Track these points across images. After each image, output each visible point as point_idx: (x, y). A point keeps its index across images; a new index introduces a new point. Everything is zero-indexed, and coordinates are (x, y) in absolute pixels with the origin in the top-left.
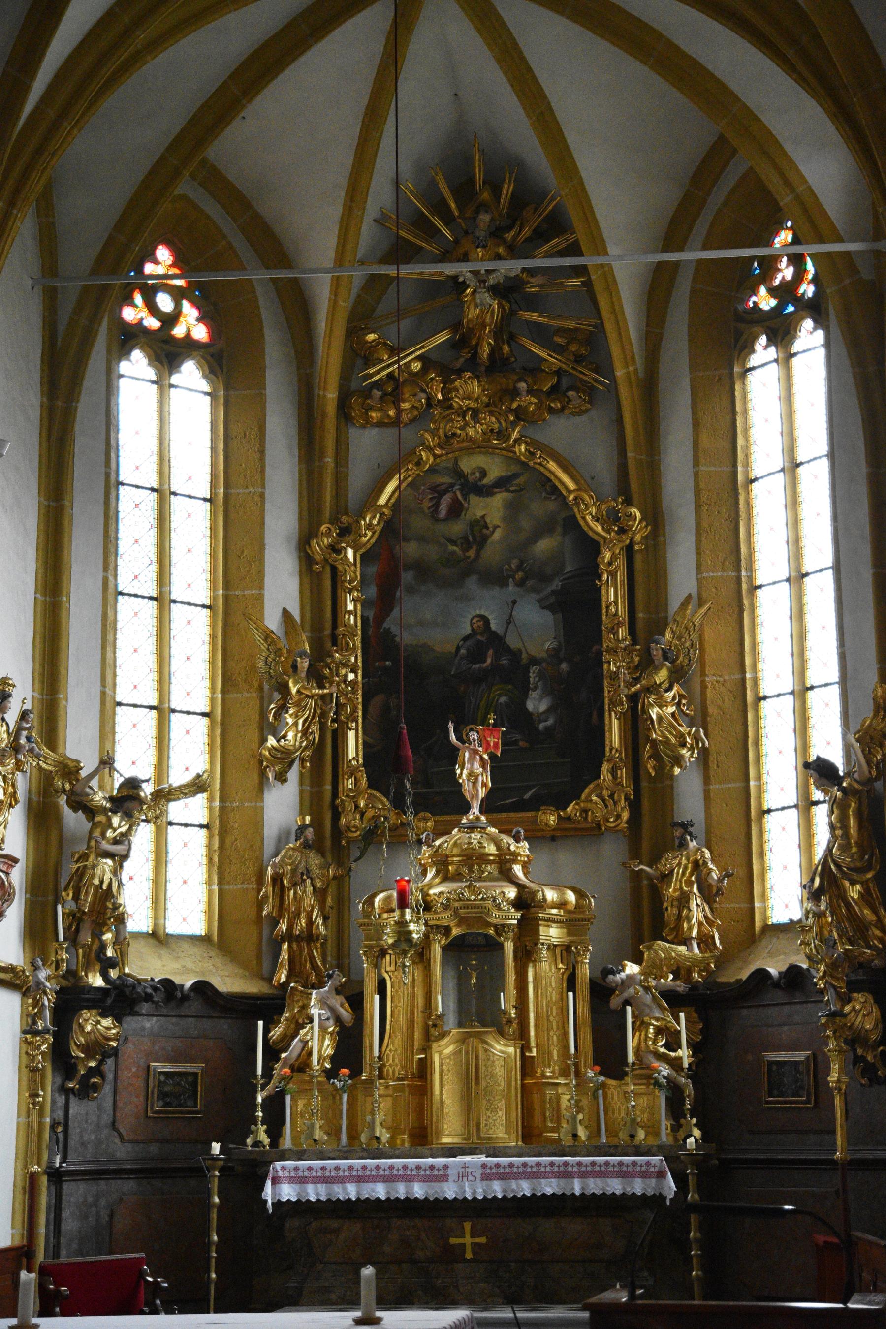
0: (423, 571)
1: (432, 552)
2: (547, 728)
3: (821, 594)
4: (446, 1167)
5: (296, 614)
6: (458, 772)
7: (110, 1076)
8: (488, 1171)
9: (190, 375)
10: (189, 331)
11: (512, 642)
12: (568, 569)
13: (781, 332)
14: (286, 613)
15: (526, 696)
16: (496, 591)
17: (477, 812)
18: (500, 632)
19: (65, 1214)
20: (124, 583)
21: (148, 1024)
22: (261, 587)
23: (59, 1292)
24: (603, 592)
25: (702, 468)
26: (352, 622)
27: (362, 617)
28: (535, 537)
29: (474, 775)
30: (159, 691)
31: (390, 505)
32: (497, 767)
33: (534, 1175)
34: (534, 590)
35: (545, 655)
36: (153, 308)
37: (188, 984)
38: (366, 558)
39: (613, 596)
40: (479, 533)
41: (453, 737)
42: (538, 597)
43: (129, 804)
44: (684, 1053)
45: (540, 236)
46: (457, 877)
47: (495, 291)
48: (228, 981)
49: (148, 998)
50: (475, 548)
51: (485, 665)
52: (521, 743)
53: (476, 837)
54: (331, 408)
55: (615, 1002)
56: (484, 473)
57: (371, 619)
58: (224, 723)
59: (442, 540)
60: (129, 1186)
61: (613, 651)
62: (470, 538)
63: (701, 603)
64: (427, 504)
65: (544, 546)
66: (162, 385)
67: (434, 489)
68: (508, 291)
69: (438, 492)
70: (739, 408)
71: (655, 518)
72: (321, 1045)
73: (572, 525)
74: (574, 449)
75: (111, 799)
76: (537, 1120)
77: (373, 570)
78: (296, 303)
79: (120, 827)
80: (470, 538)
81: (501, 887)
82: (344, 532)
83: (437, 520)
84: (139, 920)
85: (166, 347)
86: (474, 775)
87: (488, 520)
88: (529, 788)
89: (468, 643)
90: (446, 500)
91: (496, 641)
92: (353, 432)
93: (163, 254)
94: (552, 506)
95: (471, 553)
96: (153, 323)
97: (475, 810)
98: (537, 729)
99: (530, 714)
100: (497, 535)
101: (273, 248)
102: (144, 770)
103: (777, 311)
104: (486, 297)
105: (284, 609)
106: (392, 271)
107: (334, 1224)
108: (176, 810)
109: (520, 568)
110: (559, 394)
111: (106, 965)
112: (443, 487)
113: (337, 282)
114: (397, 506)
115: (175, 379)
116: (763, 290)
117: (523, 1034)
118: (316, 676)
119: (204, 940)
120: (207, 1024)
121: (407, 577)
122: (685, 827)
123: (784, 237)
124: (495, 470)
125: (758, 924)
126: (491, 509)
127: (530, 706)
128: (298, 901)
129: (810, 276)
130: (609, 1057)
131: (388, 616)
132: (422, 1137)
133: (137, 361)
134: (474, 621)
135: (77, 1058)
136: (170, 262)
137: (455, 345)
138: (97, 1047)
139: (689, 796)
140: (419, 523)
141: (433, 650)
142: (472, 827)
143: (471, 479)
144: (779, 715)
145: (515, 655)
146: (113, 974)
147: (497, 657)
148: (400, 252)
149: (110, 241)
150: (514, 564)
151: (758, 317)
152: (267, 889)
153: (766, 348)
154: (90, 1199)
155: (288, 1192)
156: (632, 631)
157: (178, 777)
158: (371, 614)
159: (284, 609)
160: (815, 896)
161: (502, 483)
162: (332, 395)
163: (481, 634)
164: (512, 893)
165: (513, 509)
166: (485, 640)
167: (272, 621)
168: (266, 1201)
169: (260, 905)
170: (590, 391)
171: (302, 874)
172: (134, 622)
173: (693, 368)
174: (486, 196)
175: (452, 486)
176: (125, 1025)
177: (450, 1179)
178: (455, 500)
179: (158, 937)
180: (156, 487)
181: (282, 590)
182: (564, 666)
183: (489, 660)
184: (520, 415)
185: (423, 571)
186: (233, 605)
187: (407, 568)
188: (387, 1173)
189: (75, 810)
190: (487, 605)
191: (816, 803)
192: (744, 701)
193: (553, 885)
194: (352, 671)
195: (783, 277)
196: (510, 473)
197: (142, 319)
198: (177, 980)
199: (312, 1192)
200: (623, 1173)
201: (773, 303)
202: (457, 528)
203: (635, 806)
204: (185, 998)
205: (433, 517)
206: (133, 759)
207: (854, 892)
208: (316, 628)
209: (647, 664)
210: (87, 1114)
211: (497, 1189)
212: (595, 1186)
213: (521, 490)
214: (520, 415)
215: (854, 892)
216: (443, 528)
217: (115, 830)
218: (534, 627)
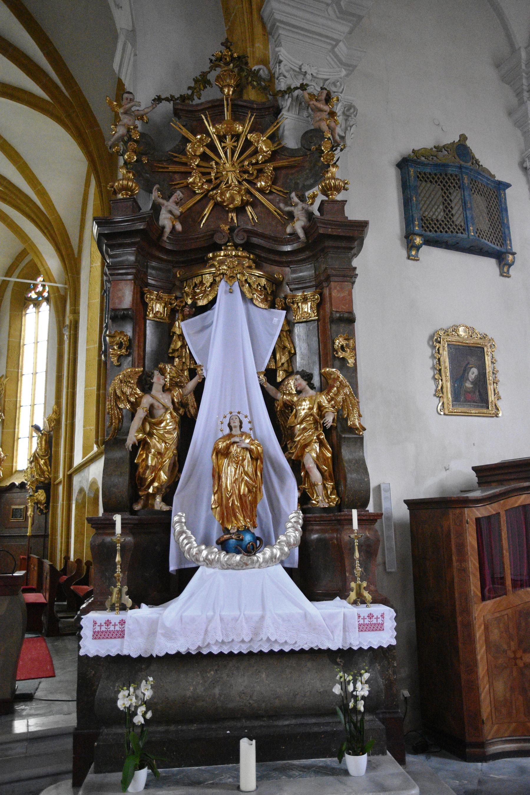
9: (45, 307)
13: (37, 304)
63: (6, 377)
103: (37, 299)
151: (30, 300)
160: (31, 463)
173: (10, 311)
207: (42, 462)
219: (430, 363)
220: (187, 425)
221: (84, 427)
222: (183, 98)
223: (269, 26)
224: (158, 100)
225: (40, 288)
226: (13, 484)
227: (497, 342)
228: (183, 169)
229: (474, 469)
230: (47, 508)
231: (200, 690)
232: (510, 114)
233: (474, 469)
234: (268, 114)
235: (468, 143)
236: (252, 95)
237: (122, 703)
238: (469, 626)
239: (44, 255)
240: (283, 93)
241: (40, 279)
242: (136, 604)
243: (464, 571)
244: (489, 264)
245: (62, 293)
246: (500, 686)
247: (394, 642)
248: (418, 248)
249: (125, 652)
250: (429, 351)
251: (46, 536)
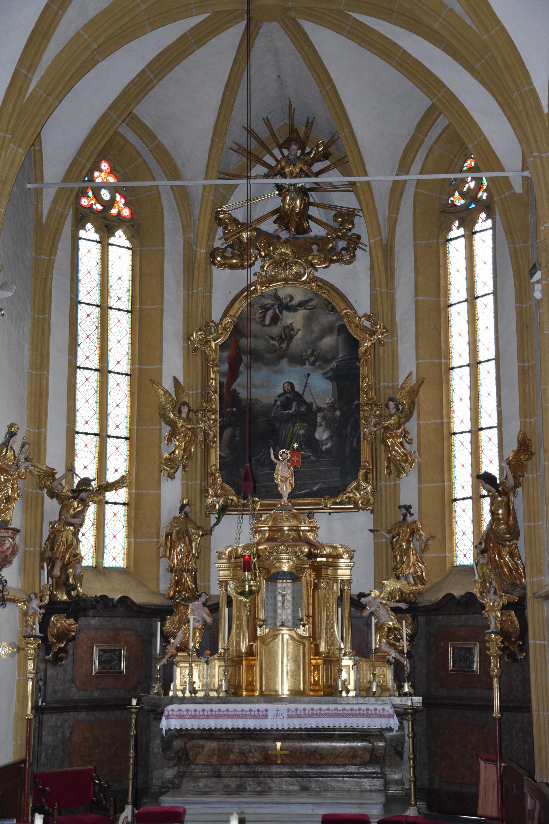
2: (326, 449)
3: (488, 374)
4: (266, 710)
5: (181, 379)
6: (276, 477)
7: (71, 652)
8: (291, 713)
9: (120, 238)
10: (119, 211)
11: (308, 398)
12: (340, 356)
14: (175, 380)
15: (315, 430)
16: (298, 368)
17: (286, 501)
18: (301, 392)
19: (45, 733)
20: (81, 361)
21: (94, 622)
22: (161, 364)
23: (45, 790)
24: (361, 368)
25: (420, 298)
26: (214, 384)
27: (220, 382)
28: (322, 336)
29: (284, 476)
30: (100, 427)
31: (237, 315)
34: (320, 367)
35: (326, 406)
36: (98, 198)
37: (117, 597)
40: (288, 334)
41: (272, 456)
42: (322, 372)
43: (83, 495)
44: (405, 644)
49: (93, 607)
50: (286, 342)
51: (291, 411)
52: (312, 458)
56: (292, 298)
57: (225, 383)
58: (137, 442)
59: (267, 337)
60: (83, 715)
62: (284, 336)
64: (258, 316)
65: (328, 341)
66: (104, 245)
67: (263, 307)
70: (441, 263)
75: (73, 491)
77: (226, 354)
79: (78, 507)
80: (284, 336)
81: (300, 545)
83: (265, 326)
84: (88, 560)
85: (106, 221)
86: (284, 476)
87: (293, 325)
88: (316, 484)
89: (281, 398)
90: (270, 314)
91: (298, 397)
95: (284, 345)
98: (321, 450)
99: (317, 441)
100: (299, 335)
102: (91, 473)
103: (465, 207)
105: (174, 377)
107: (201, 742)
108: (110, 496)
109: (312, 355)
111: (69, 588)
112: (268, 306)
115: (112, 240)
116: (457, 194)
123: (470, 163)
125: (448, 566)
126: (295, 319)
127: (317, 436)
129: (485, 187)
131: (235, 381)
133: (89, 230)
134: (286, 385)
135: (52, 642)
136: (109, 171)
138: (62, 635)
140: (255, 327)
141: (261, 402)
143: (284, 301)
144: (462, 444)
145: (309, 406)
146: (73, 593)
147: (298, 406)
150: (309, 352)
153: (458, 228)
154: (59, 724)
155: (175, 724)
157: (112, 477)
158: (225, 380)
159: (174, 377)
161: (302, 304)
163: (290, 393)
165: (309, 320)
166: (292, 396)
167: (168, 384)
168: (162, 729)
171: (183, 533)
172: (87, 385)
175: (273, 305)
176: (80, 623)
177: (269, 717)
178: (275, 314)
179: (99, 569)
180: (99, 304)
181: (173, 364)
182: (338, 413)
183: (294, 409)
185: (256, 356)
186: (143, 376)
187: (245, 353)
188: (233, 713)
189: (52, 497)
190: (292, 376)
191: (484, 496)
194: (213, 414)
195: (469, 187)
196: (307, 299)
197: (92, 204)
198: (110, 596)
201: (463, 202)
202: (276, 330)
204: (114, 606)
205: (262, 323)
206: (85, 466)
210: (57, 674)
213: (314, 308)
216: (267, 329)
217: (75, 509)
218: (320, 389)
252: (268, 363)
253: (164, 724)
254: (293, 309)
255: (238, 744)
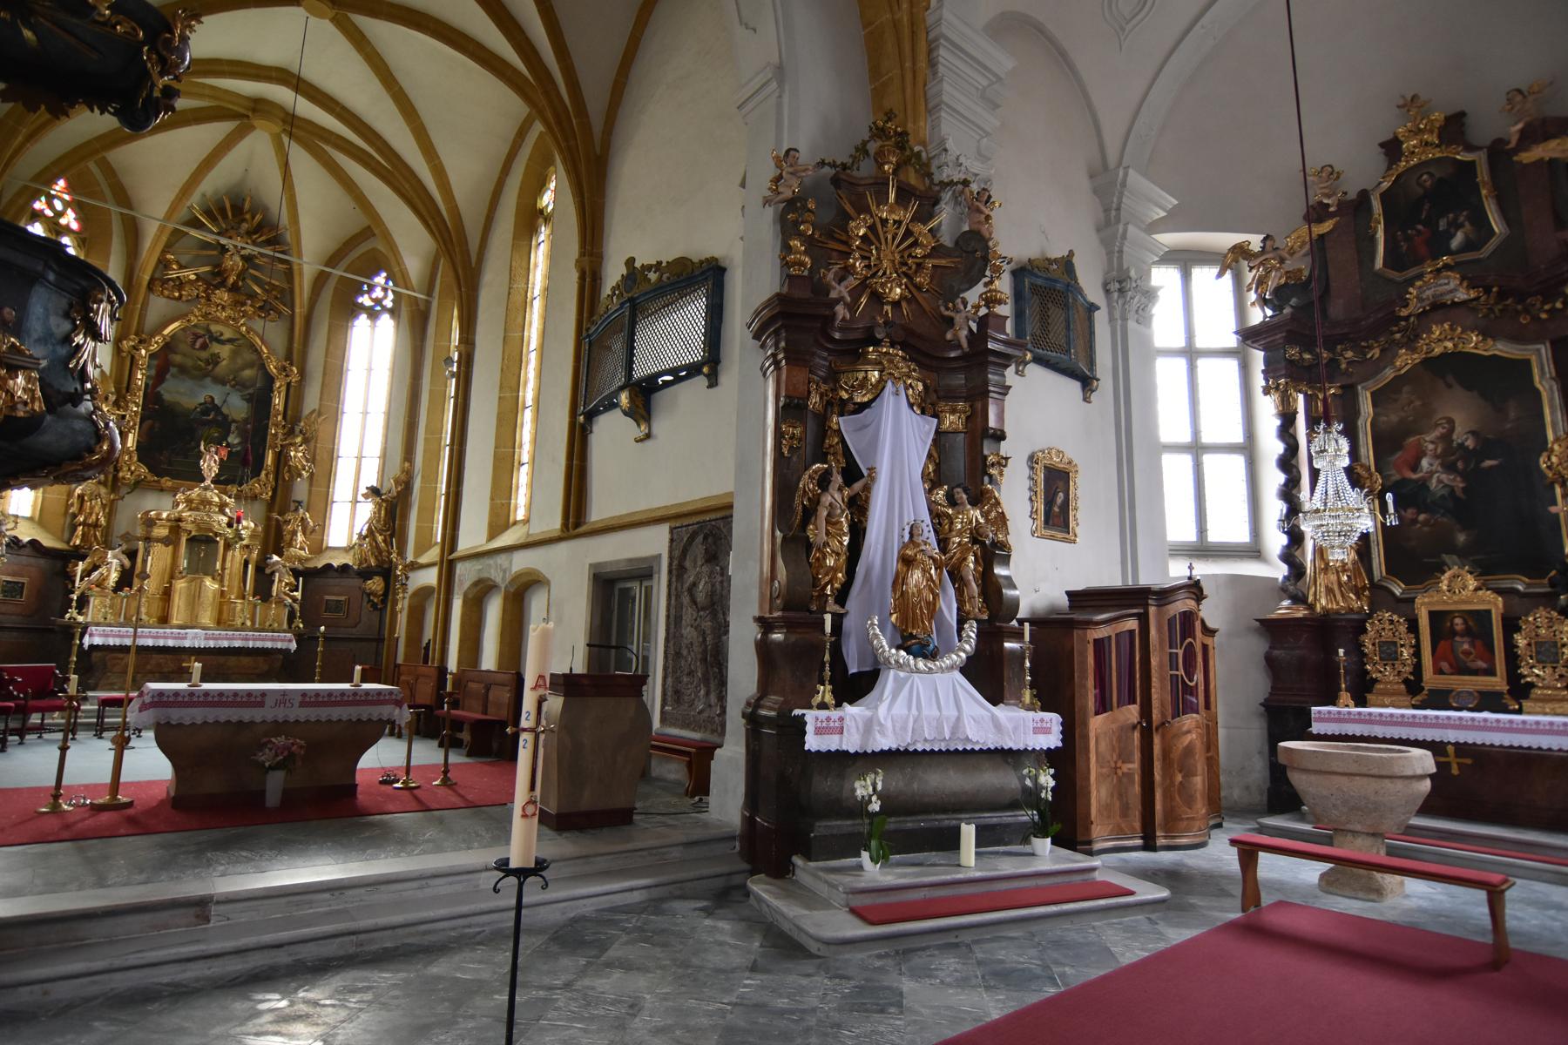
0: (183, 370)
1: (189, 362)
9: (386, 322)
11: (225, 410)
16: (219, 387)
29: (210, 465)
32: (222, 463)
33: (156, 637)
36: (51, 206)
37: (26, 539)
38: (152, 356)
39: (278, 401)
40: (215, 360)
44: (298, 595)
45: (268, 243)
46: (197, 509)
47: (243, 258)
48: (48, 541)
53: (209, 494)
54: (145, 283)
55: (268, 571)
61: (276, 425)
65: (248, 373)
68: (247, 259)
69: (197, 337)
71: (302, 372)
72: (114, 576)
73: (263, 367)
74: (269, 336)
76: (225, 616)
77: (155, 362)
78: (133, 232)
82: (141, 342)
86: (210, 465)
90: (200, 341)
91: (217, 409)
92: (152, 296)
93: (61, 183)
94: (254, 357)
96: (49, 213)
97: (208, 482)
101: (123, 197)
103: (371, 308)
104: (237, 258)
106: (185, 229)
110: (265, 309)
113: (162, 229)
114: (174, 336)
117: (222, 581)
118: (116, 404)
119: (31, 519)
120: (32, 560)
121: (173, 370)
122: (300, 503)
124: (228, 334)
126: (225, 351)
128: (92, 508)
130: (263, 587)
132: (164, 620)
137: (214, 274)
139: (300, 490)
140: (183, 347)
142: (206, 489)
145: (225, 417)
148: (195, 223)
149: (47, 168)
151: (362, 308)
152: (74, 500)
155: (98, 641)
156: (284, 418)
161: (230, 341)
162: (147, 277)
164: (225, 519)
165: (235, 354)
169: (68, 507)
170: (279, 313)
173: (332, 317)
174: (248, 216)
184: (245, 314)
185: (183, 370)
190: (216, 393)
192: (331, 457)
193: (236, 519)
199: (111, 642)
200: (273, 640)
202: (204, 355)
203: (274, 490)
204: (24, 546)
207: (380, 538)
208: (118, 383)
209: (291, 433)
211: (211, 644)
212: (259, 644)
214: (245, 314)
215: (380, 538)
216: (198, 353)
218: (237, 407)
219: (1027, 483)
220: (858, 532)
221: (492, 499)
222: (844, 166)
223: (931, 105)
224: (822, 163)
225: (378, 293)
226: (329, 566)
227: (1080, 468)
228: (843, 248)
229: (1068, 593)
230: (384, 601)
231: (901, 784)
232: (1098, 230)
233: (1068, 593)
234: (927, 205)
235: (1075, 260)
236: (912, 178)
237: (860, 792)
238: (1086, 737)
239: (401, 250)
240: (945, 185)
241: (380, 279)
242: (838, 705)
243: (1085, 686)
244: (1075, 386)
245: (422, 307)
246: (1104, 792)
247: (1060, 744)
248: (1026, 364)
249: (845, 748)
250: (1027, 471)
251: (380, 640)
252: (193, 378)
253: (87, 641)
254: (223, 342)
255: (157, 658)
